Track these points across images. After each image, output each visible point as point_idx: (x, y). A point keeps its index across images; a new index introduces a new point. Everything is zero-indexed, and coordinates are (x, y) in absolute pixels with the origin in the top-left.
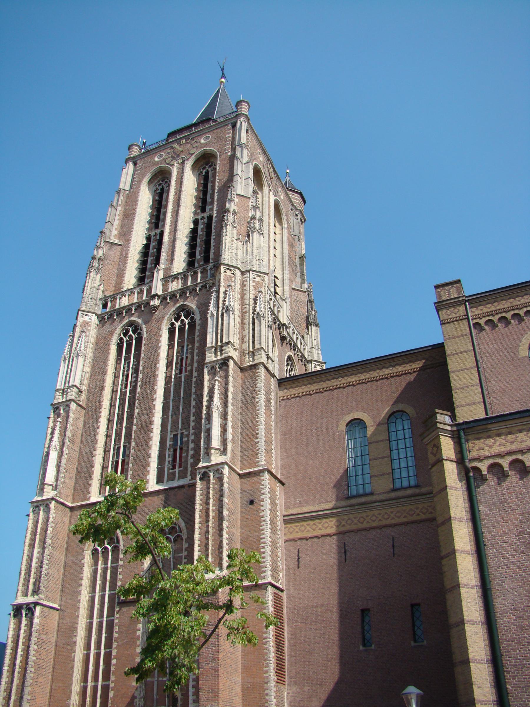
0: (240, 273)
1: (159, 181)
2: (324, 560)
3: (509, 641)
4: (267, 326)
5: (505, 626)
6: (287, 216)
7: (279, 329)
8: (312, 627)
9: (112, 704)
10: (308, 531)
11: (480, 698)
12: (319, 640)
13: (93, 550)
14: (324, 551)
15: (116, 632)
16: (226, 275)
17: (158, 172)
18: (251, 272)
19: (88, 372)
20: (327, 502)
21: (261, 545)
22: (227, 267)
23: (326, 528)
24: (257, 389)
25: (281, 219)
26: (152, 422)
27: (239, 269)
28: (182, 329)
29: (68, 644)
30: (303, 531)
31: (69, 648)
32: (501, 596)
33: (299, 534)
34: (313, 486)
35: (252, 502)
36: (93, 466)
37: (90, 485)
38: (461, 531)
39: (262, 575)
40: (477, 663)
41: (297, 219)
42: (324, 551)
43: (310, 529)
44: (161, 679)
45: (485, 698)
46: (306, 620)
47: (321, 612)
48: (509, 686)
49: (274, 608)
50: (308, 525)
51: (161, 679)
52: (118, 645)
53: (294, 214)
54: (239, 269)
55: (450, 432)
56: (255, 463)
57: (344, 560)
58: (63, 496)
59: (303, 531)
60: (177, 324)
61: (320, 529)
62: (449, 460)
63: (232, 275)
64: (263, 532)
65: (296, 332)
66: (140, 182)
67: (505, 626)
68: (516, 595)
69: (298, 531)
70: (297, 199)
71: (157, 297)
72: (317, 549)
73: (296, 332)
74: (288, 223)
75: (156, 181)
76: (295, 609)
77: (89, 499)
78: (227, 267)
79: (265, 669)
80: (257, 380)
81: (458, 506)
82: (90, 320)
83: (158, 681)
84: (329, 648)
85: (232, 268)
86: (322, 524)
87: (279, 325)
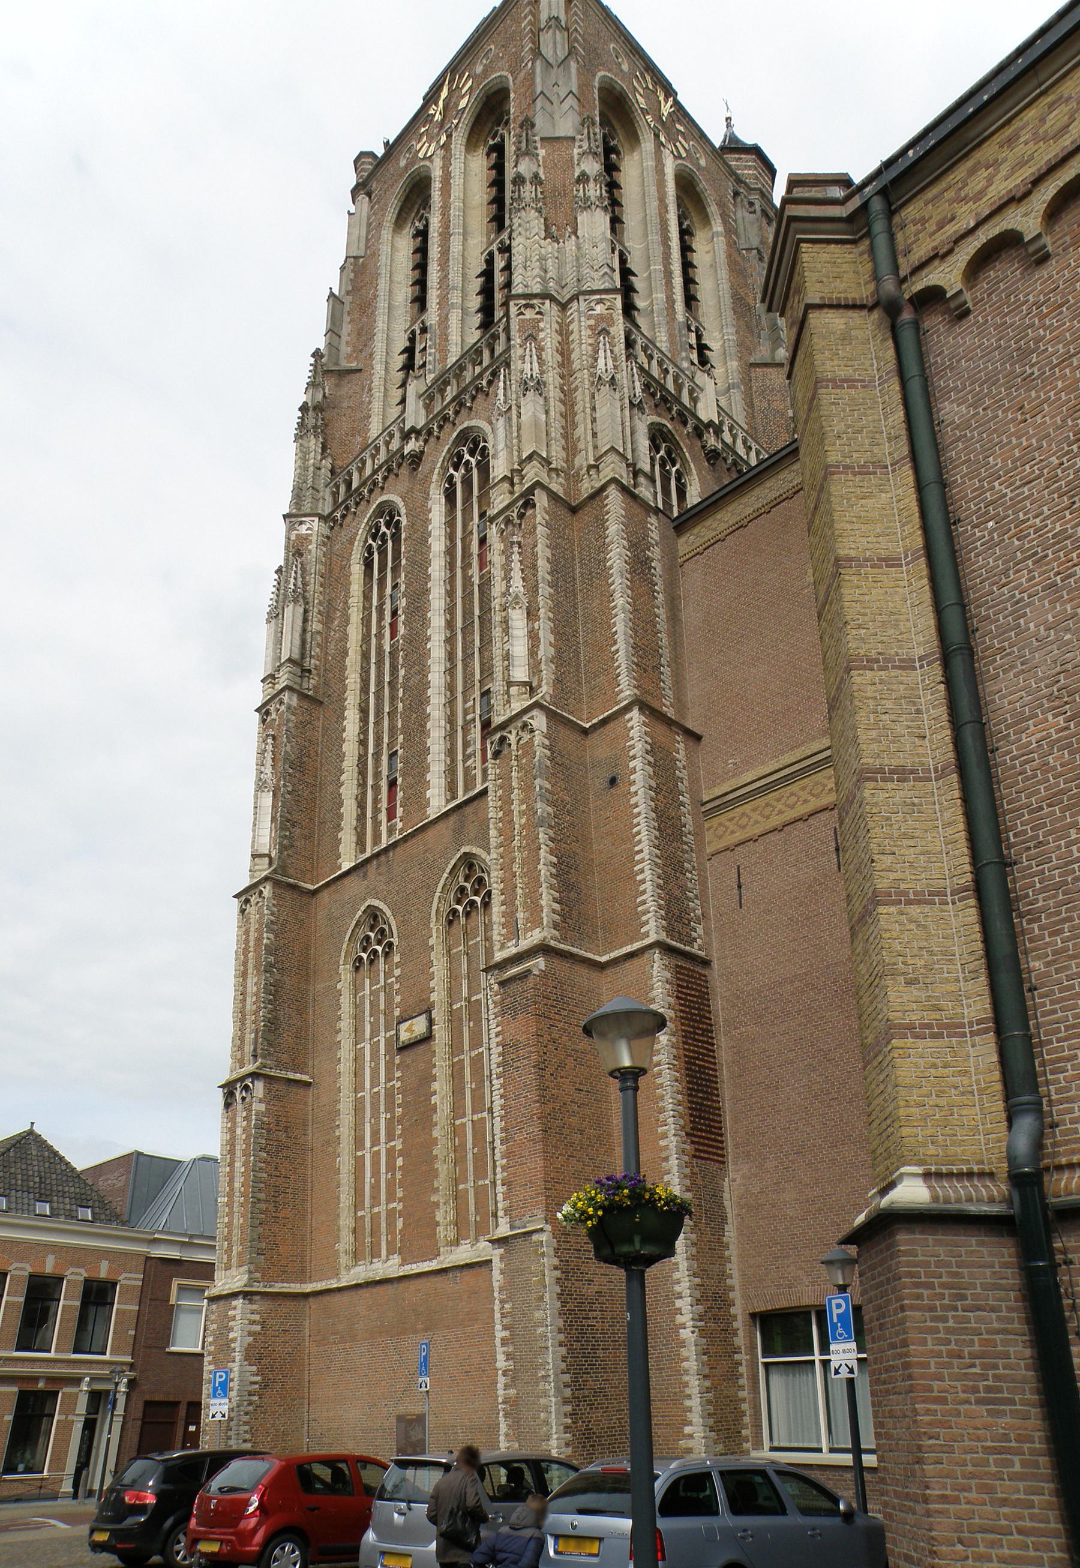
0: (555, 308)
1: (418, 212)
2: (794, 876)
3: (1041, 808)
4: (627, 404)
5: (1027, 762)
6: (721, 205)
7: (700, 436)
8: (775, 1030)
9: (401, 1241)
10: (756, 822)
11: (914, 1017)
12: (791, 1055)
13: (354, 962)
14: (792, 859)
15: (399, 1106)
16: (523, 321)
17: (411, 191)
18: (581, 298)
19: (319, 632)
20: (792, 749)
21: (636, 869)
22: (524, 302)
23: (792, 807)
24: (607, 540)
25: (707, 216)
26: (427, 685)
27: (553, 299)
28: (467, 482)
29: (328, 1142)
30: (744, 827)
31: (330, 1149)
32: (1012, 667)
33: (738, 834)
34: (759, 724)
35: (613, 781)
36: (341, 804)
37: (339, 842)
38: (870, 502)
39: (642, 930)
40: (909, 903)
41: (754, 212)
42: (792, 859)
43: (760, 818)
44: (481, 1183)
45: (936, 1015)
46: (760, 1017)
47: (793, 994)
48: (1036, 964)
49: (678, 998)
50: (754, 810)
51: (481, 1183)
52: (403, 1130)
53: (746, 204)
54: (553, 299)
55: (841, 226)
56: (614, 699)
57: (836, 867)
58: (291, 871)
59: (744, 827)
60: (458, 476)
61: (780, 812)
62: (831, 306)
63: (539, 316)
64: (637, 838)
65: (754, 446)
66: (380, 226)
67: (1027, 762)
68: (1070, 642)
69: (735, 828)
70: (749, 168)
71: (413, 435)
72: (776, 857)
73: (754, 446)
74: (725, 222)
75: (413, 214)
76: (738, 997)
77: (340, 868)
78: (524, 302)
79: (660, 1130)
80: (607, 520)
81: (860, 432)
82: (309, 532)
83: (476, 1187)
84: (815, 1070)
85: (535, 301)
86: (783, 801)
87: (696, 428)
